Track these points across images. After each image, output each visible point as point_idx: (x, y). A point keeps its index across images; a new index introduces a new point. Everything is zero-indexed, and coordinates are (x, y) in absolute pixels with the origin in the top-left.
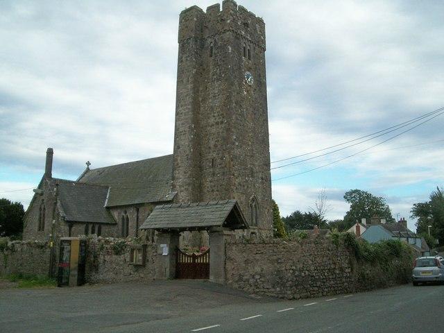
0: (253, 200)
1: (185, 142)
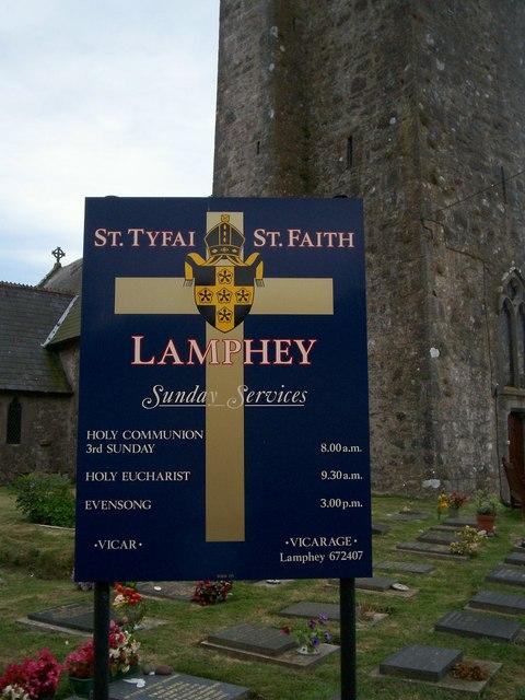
1: (251, 94)
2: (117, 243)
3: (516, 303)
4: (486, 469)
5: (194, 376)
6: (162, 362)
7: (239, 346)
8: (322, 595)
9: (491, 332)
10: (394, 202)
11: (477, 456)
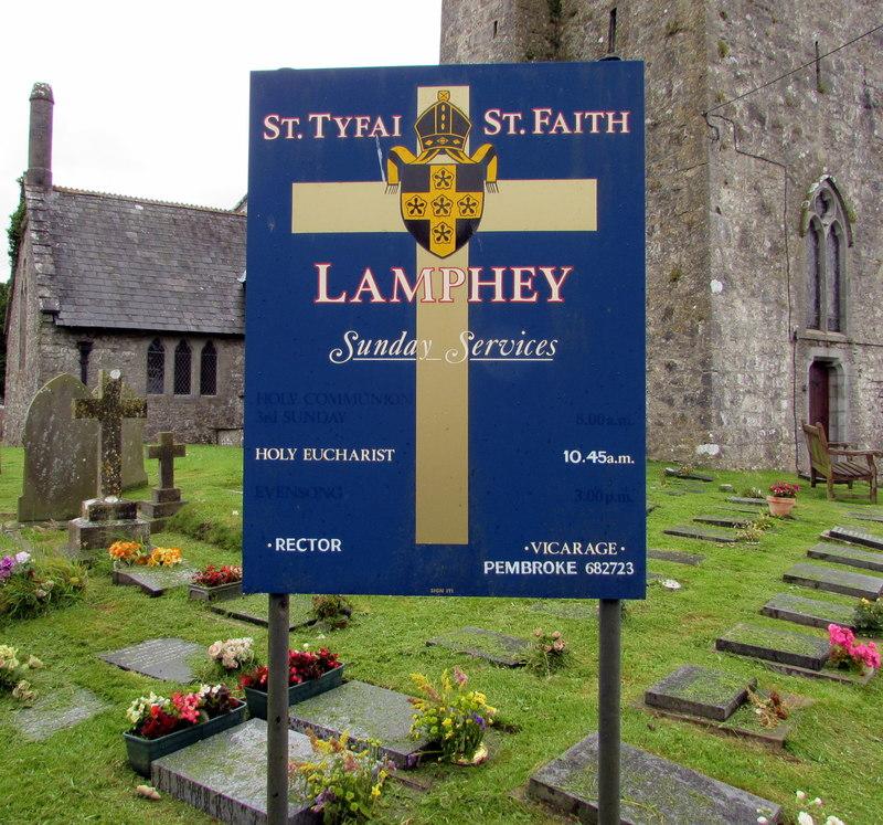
2: (295, 134)
3: (827, 221)
4: (776, 437)
5: (399, 319)
6: (357, 299)
7: (461, 277)
8: (568, 623)
9: (792, 259)
10: (669, 93)
11: (768, 418)
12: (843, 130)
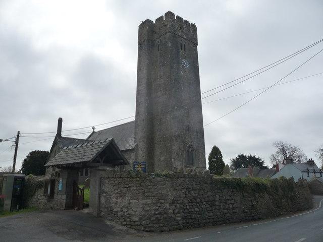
0: (190, 147)
12: (193, 137)
